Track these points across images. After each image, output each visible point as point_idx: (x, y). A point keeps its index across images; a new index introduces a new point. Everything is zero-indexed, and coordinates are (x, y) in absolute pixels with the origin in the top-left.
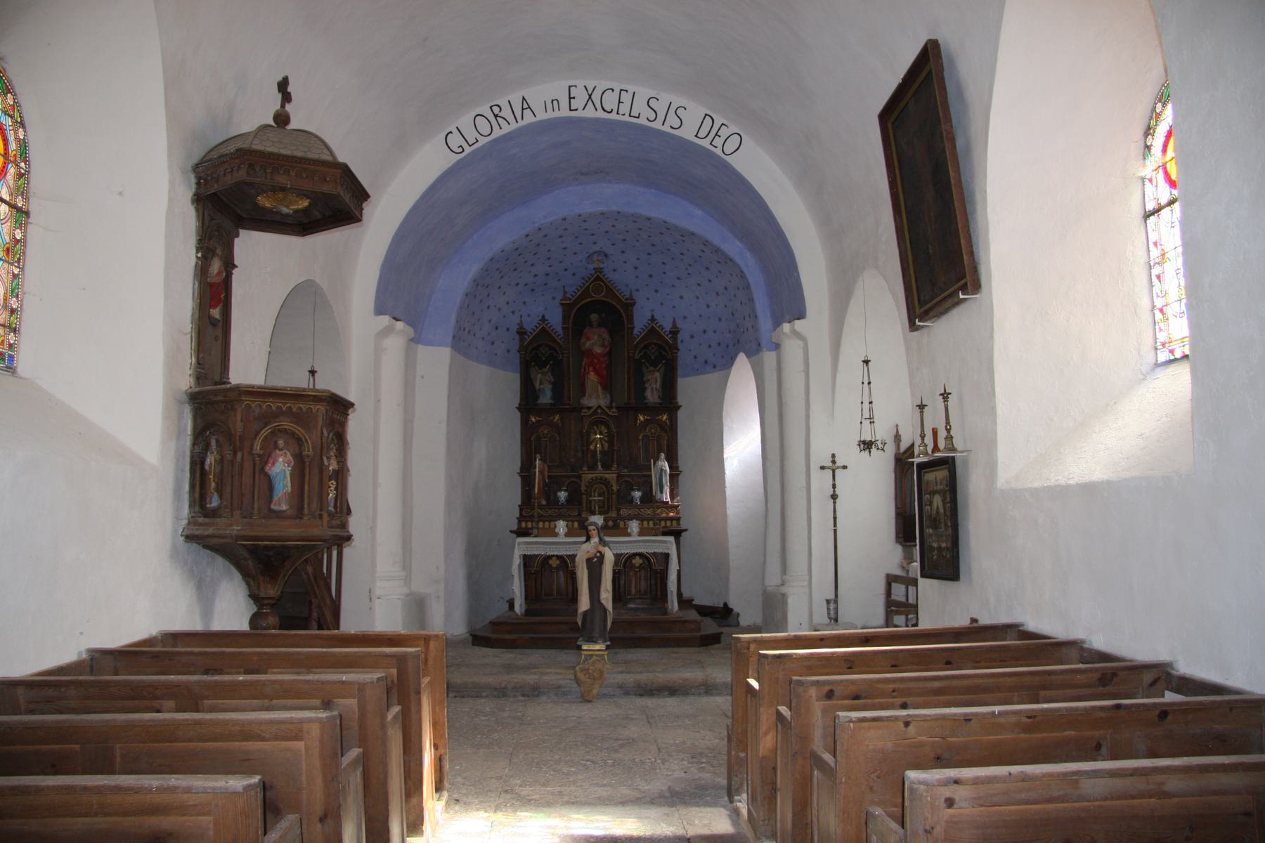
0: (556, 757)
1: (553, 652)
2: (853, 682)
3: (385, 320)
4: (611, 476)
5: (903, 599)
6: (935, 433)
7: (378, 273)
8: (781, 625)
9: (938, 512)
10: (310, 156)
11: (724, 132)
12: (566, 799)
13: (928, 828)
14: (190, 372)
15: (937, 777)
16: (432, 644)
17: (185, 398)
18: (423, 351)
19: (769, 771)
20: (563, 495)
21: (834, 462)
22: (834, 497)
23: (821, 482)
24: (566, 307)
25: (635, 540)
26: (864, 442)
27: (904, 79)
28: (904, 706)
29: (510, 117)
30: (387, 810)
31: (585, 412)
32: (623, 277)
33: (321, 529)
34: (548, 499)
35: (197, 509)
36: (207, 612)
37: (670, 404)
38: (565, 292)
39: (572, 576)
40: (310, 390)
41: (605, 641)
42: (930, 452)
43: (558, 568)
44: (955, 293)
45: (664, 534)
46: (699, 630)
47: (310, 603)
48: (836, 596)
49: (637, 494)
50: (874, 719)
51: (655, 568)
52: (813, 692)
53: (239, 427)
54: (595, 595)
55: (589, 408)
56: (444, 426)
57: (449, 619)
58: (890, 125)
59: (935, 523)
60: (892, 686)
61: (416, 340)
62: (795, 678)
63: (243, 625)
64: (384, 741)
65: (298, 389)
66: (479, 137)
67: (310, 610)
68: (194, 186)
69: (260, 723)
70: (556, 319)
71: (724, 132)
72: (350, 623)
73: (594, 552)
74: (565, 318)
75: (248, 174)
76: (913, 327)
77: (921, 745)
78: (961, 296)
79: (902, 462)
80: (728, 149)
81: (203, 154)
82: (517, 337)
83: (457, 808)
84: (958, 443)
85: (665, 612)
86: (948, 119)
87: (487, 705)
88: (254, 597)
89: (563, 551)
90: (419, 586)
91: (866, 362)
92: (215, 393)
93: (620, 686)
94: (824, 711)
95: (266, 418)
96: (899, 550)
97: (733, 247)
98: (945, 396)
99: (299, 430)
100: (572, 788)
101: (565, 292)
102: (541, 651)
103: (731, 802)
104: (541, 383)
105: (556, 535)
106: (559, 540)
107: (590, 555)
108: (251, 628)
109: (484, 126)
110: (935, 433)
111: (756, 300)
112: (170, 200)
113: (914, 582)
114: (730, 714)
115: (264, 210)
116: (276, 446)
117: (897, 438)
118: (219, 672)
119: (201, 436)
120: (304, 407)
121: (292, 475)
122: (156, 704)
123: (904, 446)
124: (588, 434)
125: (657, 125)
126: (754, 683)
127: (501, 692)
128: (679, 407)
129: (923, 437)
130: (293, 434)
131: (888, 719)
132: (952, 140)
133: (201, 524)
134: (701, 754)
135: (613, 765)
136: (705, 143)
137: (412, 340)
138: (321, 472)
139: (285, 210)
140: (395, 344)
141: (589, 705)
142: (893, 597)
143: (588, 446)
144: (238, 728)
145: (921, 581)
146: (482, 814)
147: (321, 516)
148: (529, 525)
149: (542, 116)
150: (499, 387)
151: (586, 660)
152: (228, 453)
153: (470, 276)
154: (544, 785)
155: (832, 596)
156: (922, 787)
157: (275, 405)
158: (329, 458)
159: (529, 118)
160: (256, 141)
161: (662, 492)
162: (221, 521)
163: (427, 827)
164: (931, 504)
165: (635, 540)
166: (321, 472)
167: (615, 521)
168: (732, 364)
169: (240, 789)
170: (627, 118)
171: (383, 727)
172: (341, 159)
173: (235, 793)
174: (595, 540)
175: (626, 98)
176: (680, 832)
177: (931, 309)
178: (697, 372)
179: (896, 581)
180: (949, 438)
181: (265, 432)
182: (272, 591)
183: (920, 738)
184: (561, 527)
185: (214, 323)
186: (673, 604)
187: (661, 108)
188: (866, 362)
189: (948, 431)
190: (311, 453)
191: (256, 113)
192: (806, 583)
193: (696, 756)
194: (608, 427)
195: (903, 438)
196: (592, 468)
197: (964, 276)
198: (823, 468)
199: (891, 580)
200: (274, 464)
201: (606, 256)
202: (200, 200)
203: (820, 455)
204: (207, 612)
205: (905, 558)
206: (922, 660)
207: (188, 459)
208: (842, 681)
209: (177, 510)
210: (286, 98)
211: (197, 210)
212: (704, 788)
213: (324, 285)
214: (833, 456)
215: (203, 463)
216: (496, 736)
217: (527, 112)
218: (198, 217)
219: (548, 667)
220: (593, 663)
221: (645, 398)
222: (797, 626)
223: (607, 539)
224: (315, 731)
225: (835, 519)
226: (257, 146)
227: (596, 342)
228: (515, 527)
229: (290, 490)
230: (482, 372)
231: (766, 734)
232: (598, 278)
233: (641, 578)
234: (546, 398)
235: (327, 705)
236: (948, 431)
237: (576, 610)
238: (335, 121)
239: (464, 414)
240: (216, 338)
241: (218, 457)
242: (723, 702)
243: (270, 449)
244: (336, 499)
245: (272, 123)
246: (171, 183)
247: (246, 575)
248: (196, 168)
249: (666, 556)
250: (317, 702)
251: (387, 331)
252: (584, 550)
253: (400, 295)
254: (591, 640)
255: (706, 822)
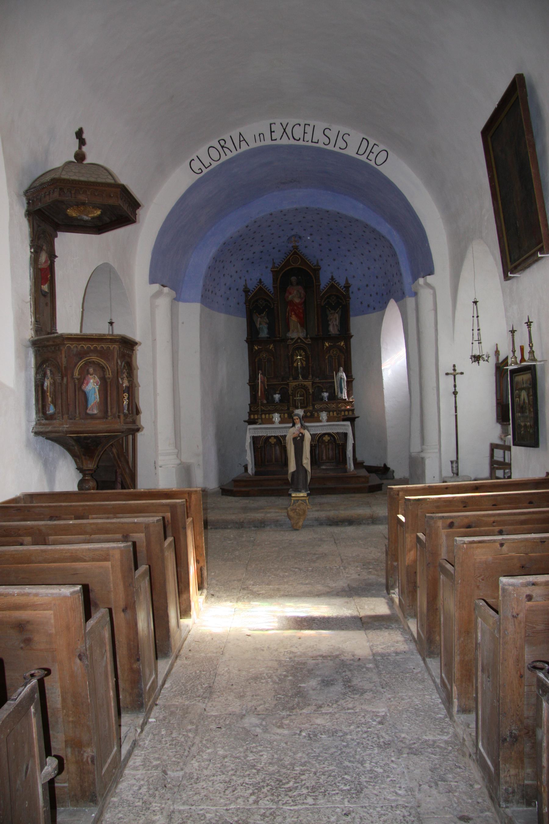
0: (276, 566)
1: (273, 498)
2: (467, 517)
3: (156, 287)
4: (308, 384)
5: (502, 460)
6: (522, 349)
7: (150, 256)
8: (421, 478)
9: (524, 402)
10: (99, 180)
11: (376, 150)
12: (282, 593)
13: (515, 614)
14: (31, 327)
15: (521, 581)
16: (193, 497)
17: (29, 344)
18: (182, 306)
19: (412, 573)
20: (277, 397)
21: (454, 370)
22: (455, 393)
23: (446, 384)
24: (275, 273)
25: (324, 425)
26: (474, 356)
27: (498, 105)
28: (501, 533)
29: (232, 147)
30: (167, 603)
31: (289, 342)
32: (312, 249)
33: (119, 425)
34: (267, 399)
35: (41, 415)
36: (51, 480)
37: (345, 334)
38: (274, 263)
39: (284, 449)
40: (109, 335)
41: (306, 491)
42: (518, 362)
43: (275, 444)
44: (535, 254)
45: (344, 420)
46: (368, 482)
47: (116, 472)
48: (457, 458)
49: (326, 395)
50: (480, 542)
51: (338, 443)
52: (440, 523)
53: (63, 361)
54: (299, 462)
55: (292, 339)
56: (198, 355)
57: (206, 478)
58: (489, 139)
59: (522, 409)
60: (492, 519)
61: (177, 299)
62: (428, 515)
63: (73, 487)
64: (163, 560)
65: (100, 335)
66: (212, 162)
67: (116, 476)
68: (26, 205)
69: (83, 550)
70: (268, 282)
71: (376, 150)
72: (143, 483)
73: (298, 433)
74: (275, 280)
75: (60, 195)
76: (506, 278)
77: (512, 558)
78: (539, 256)
79: (500, 369)
80: (379, 161)
81: (30, 183)
82: (243, 294)
83: (213, 599)
84: (537, 355)
85: (345, 470)
86: (531, 132)
87: (231, 533)
88: (80, 469)
89: (278, 433)
90: (186, 458)
91: (475, 302)
92: (48, 340)
93: (317, 520)
94: (448, 536)
95: (81, 355)
96: (498, 427)
97: (384, 228)
98: (529, 324)
99: (103, 362)
100: (286, 586)
101: (274, 263)
102: (266, 498)
103: (388, 593)
104: (260, 324)
105: (273, 423)
106: (274, 426)
107: (295, 435)
108: (79, 489)
109: (215, 155)
110: (522, 349)
111: (400, 263)
112: (11, 215)
113: (509, 449)
114: (387, 537)
115: (72, 218)
116: (88, 373)
117: (497, 353)
118: (59, 518)
119: (40, 368)
120: (105, 346)
121: (99, 391)
122: (20, 539)
123: (501, 359)
124: (292, 356)
125: (330, 147)
126: (402, 518)
127: (240, 525)
128: (352, 336)
129: (514, 351)
130: (99, 364)
131: (489, 541)
132: (533, 146)
133: (44, 425)
134: (369, 563)
135: (312, 571)
136: (363, 158)
137: (175, 299)
138: (118, 388)
139: (85, 218)
140: (164, 303)
141: (297, 532)
142: (495, 458)
143: (293, 364)
144: (68, 554)
145: (513, 448)
146: (229, 603)
147: (119, 417)
148: (256, 417)
149: (253, 145)
150: (233, 328)
151: (294, 503)
152: (58, 378)
153: (211, 255)
154: (268, 584)
155: (454, 459)
156: (511, 588)
157: (86, 346)
158: (122, 379)
159: (244, 147)
160: (64, 173)
161: (342, 393)
162: (56, 422)
163: (193, 612)
164: (519, 397)
165: (324, 425)
166: (118, 388)
167: (311, 413)
168: (386, 307)
169: (69, 594)
170: (310, 144)
171: (162, 551)
172: (123, 180)
173: (65, 597)
174: (298, 425)
175: (309, 130)
176: (355, 613)
177: (519, 265)
178: (363, 313)
179: (497, 448)
180: (532, 352)
181: (81, 363)
182: (90, 465)
183: (510, 554)
184: (276, 417)
185: (44, 295)
186: (351, 466)
187: (332, 135)
188: (475, 302)
189: (531, 347)
190: (111, 376)
191: (62, 154)
192: (437, 450)
193: (366, 564)
194: (305, 351)
195: (501, 353)
196: (296, 378)
197: (541, 242)
198: (447, 374)
199: (493, 447)
200: (87, 384)
201: (300, 237)
202: (29, 214)
203: (445, 366)
204: (51, 480)
205: (503, 433)
206: (512, 501)
207: (33, 384)
208: (459, 516)
209: (28, 416)
210: (82, 142)
211: (29, 221)
212: (371, 585)
213: (115, 266)
214: (454, 366)
215: (42, 385)
216: (237, 553)
217: (243, 143)
218: (30, 225)
219: (270, 508)
220: (299, 505)
221: (329, 331)
222: (432, 478)
223: (307, 424)
224: (117, 555)
225: (456, 407)
226: (65, 176)
227: (295, 295)
228: (247, 418)
229: (98, 400)
230: (221, 318)
231: (410, 550)
232: (295, 253)
233: (330, 450)
234: (264, 334)
235: (125, 538)
236: (531, 347)
237: (287, 471)
238: (115, 157)
239: (211, 346)
240: (47, 304)
241: (52, 381)
242: (383, 529)
243: (84, 373)
244: (128, 405)
245: (74, 160)
246: (11, 204)
247: (74, 456)
248: (26, 193)
249: (345, 435)
250: (119, 536)
251: (157, 295)
252: (291, 432)
253: (166, 270)
254: (297, 490)
255: (372, 607)
